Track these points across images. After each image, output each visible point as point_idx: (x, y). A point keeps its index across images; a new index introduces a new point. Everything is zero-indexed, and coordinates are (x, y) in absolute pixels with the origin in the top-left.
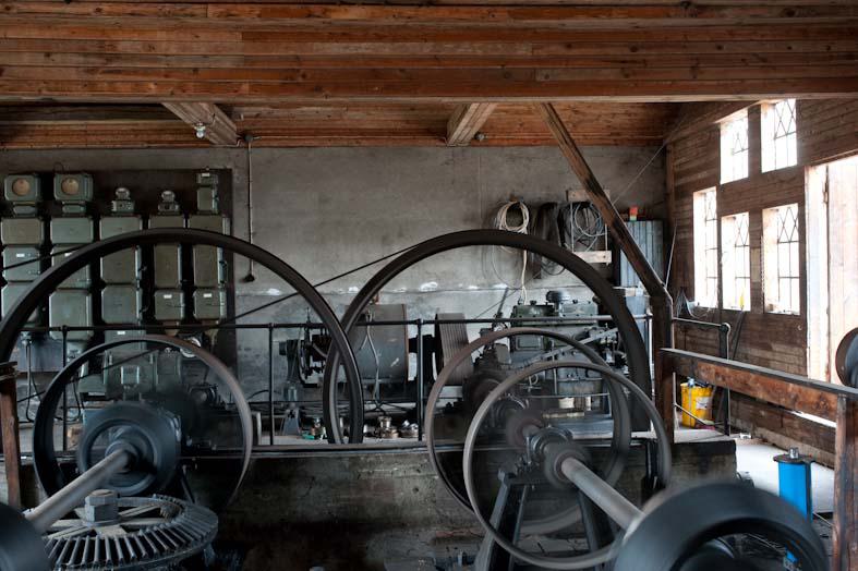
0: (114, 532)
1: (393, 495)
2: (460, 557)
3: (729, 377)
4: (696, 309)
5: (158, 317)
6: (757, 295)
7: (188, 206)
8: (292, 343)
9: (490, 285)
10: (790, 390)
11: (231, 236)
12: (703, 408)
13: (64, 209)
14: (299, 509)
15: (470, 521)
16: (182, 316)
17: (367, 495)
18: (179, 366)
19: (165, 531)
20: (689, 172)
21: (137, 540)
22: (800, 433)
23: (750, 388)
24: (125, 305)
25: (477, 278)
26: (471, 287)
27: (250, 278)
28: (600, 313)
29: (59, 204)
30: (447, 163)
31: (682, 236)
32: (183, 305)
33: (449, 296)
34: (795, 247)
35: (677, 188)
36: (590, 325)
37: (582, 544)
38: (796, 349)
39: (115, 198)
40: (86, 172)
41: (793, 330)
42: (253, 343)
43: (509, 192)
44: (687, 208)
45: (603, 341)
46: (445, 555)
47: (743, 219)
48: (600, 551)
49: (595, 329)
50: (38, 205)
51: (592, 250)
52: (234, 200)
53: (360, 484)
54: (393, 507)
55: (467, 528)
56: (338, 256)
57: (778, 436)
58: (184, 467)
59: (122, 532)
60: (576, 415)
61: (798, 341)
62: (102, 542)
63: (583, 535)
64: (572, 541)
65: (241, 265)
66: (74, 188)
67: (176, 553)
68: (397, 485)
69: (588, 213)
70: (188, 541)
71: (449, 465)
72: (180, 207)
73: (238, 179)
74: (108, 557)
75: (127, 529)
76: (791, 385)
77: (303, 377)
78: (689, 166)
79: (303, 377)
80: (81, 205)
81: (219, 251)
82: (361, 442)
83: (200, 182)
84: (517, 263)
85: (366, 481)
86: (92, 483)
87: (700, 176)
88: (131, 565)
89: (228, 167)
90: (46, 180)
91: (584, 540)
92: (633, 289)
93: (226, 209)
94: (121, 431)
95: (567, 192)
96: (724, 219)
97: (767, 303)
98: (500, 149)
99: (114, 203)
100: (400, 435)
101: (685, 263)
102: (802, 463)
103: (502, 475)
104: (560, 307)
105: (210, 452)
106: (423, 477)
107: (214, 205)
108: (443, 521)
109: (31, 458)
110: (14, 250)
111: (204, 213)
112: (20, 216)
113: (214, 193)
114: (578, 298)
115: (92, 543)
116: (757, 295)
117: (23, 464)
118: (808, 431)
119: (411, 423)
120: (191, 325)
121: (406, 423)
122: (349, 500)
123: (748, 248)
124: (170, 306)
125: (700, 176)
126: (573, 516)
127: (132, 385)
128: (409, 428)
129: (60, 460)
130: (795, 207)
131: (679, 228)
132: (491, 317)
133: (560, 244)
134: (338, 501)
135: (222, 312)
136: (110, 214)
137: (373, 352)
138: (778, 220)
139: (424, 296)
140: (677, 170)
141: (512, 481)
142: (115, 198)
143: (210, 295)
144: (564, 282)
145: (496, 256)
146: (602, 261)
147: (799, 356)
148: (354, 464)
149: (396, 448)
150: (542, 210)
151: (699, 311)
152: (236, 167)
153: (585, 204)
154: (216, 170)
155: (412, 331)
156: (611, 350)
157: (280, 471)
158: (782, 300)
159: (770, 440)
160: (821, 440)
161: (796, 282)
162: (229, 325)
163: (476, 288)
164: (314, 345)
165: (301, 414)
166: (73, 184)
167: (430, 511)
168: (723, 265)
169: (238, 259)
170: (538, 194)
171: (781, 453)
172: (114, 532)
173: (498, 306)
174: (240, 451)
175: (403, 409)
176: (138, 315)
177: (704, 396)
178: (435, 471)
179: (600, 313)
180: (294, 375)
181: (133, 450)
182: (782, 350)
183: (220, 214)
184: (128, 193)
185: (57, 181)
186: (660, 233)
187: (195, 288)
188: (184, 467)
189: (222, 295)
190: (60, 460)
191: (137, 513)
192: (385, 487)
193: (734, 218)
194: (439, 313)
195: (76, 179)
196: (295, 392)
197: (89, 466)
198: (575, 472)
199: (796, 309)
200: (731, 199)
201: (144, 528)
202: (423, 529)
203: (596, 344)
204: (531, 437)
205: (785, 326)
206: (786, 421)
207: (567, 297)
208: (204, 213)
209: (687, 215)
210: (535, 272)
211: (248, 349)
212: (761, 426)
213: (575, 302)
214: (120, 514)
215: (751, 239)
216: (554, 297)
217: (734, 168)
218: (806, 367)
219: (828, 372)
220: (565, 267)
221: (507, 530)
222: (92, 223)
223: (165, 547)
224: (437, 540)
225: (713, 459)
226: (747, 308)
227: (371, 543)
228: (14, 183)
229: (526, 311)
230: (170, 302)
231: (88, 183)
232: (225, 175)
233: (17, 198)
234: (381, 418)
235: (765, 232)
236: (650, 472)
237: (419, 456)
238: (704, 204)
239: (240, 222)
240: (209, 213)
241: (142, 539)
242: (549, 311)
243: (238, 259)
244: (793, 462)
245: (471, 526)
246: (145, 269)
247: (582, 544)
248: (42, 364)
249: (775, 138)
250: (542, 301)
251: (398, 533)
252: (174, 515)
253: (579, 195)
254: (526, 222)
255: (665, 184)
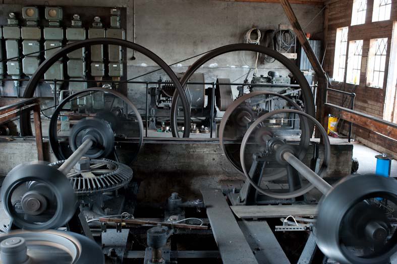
0: (88, 175)
1: (204, 161)
2: (234, 190)
3: (357, 119)
4: (333, 82)
5: (93, 74)
6: (363, 78)
7: (106, 25)
8: (153, 89)
9: (241, 66)
10: (387, 128)
11: (126, 40)
12: (333, 126)
13: (50, 23)
14: (163, 165)
15: (236, 173)
16: (103, 74)
17: (192, 161)
18: (103, 97)
19: (112, 176)
20: (336, 19)
21: (101, 179)
22: (377, 141)
23: (367, 125)
24: (77, 69)
25: (236, 62)
26: (232, 67)
27: (133, 58)
28: (291, 84)
29: (48, 21)
30: (225, 9)
31: (329, 48)
32: (104, 70)
33: (222, 70)
34: (384, 58)
35: (329, 26)
36: (287, 87)
37: (286, 186)
38: (379, 104)
39: (73, 19)
40: (60, 6)
41: (379, 95)
42: (137, 89)
43: (252, 24)
44: (333, 35)
45: (292, 95)
46: (226, 189)
47: (360, 43)
48: (295, 192)
49: (289, 89)
50: (38, 21)
51: (288, 52)
52: (127, 21)
53: (190, 156)
54: (203, 166)
55: (235, 176)
56: (173, 50)
57: (367, 141)
58: (115, 147)
59: (93, 176)
60: (277, 126)
61: (381, 100)
62: (86, 180)
63: (286, 182)
64: (281, 184)
65: (130, 53)
66: (54, 14)
67: (117, 186)
68: (205, 157)
69: (287, 35)
70: (122, 181)
71: (232, 151)
72: (103, 24)
73: (129, 12)
74: (89, 187)
75: (96, 175)
76: (389, 127)
77: (157, 103)
78: (337, 16)
79: (157, 103)
80: (57, 22)
81: (120, 47)
82: (188, 136)
83: (112, 13)
84: (254, 57)
85: (192, 155)
86: (80, 155)
87: (341, 21)
88: (99, 190)
89: (125, 6)
90: (41, 9)
91: (287, 185)
92: (307, 72)
93: (123, 26)
94: (88, 130)
95: (279, 25)
96: (350, 42)
97: (367, 82)
98: (248, 3)
99: (73, 21)
100: (200, 132)
101: (330, 60)
102: (388, 159)
103: (255, 157)
104: (274, 78)
105: (124, 139)
106: (217, 154)
107: (118, 24)
108: (224, 173)
109: (48, 139)
110: (28, 41)
111: (113, 28)
112: (30, 26)
113: (118, 19)
114: (283, 75)
115: (82, 180)
116: (363, 78)
117: (44, 141)
118: (381, 140)
119: (205, 126)
120: (107, 78)
121: (203, 127)
122: (184, 162)
123: (361, 57)
124: (98, 70)
125: (341, 21)
126: (282, 174)
127: (82, 105)
128: (204, 129)
129: (59, 140)
130: (386, 40)
131: (329, 44)
132: (243, 83)
133: (274, 49)
134: (180, 162)
135: (121, 74)
136: (70, 26)
137: (192, 94)
138: (378, 45)
139: (211, 70)
140: (329, 17)
141: (259, 160)
142: (73, 19)
143: (116, 66)
144: (274, 66)
145: (244, 55)
146: (292, 58)
147: (380, 107)
148: (187, 148)
149: (206, 141)
150: (267, 33)
151: (334, 83)
152: (128, 6)
153: (287, 31)
154: (119, 8)
155: (207, 87)
156: (295, 99)
157: (156, 148)
158: (375, 81)
159: (362, 142)
160: (387, 145)
161: (382, 74)
162: (124, 80)
163: (234, 67)
164: (163, 91)
165: (156, 120)
166: (54, 12)
167: (219, 169)
168: (348, 62)
169: (128, 49)
170: (265, 25)
171: (379, 154)
172: (88, 175)
173: (246, 76)
174: (139, 140)
175: (200, 119)
176: (84, 73)
177: (334, 121)
178: (223, 152)
179: (291, 84)
180: (153, 102)
181: (95, 139)
182: (373, 104)
183: (121, 28)
184: (79, 17)
185: (46, 10)
186: (319, 46)
187: (109, 62)
188: (115, 147)
189: (121, 66)
190: (59, 140)
191: (97, 167)
192: (201, 158)
193: (342, 29)
194: (219, 77)
195: (55, 10)
196: (154, 111)
197: (76, 148)
198: (287, 157)
199: (381, 86)
200: (355, 33)
201: (103, 174)
202: (216, 176)
203: (289, 96)
204: (269, 141)
205: (375, 93)
206: (371, 135)
207: (277, 74)
208: (113, 28)
209: (333, 38)
210: (262, 61)
211: (132, 90)
212: (359, 136)
213: (280, 77)
214: (91, 167)
215: (363, 53)
216: (272, 74)
217: (358, 18)
218: (383, 112)
219: (392, 115)
220: (276, 59)
221: (256, 179)
222: (62, 30)
223: (113, 183)
224: (221, 181)
225: (343, 152)
226: (358, 83)
227: (193, 181)
228: (27, 10)
229: (258, 80)
230: (98, 68)
231: (61, 11)
232: (123, 10)
233: (29, 18)
234: (192, 124)
235: (370, 50)
236: (315, 156)
237: (216, 145)
238: (342, 34)
239: (129, 32)
240: (116, 28)
241: (102, 179)
242: (269, 80)
243: (128, 49)
244: (385, 159)
245: (237, 176)
246: (87, 52)
247: (286, 186)
248: (41, 95)
249: (380, 6)
250: (266, 75)
251: (205, 177)
252: (114, 168)
253: (286, 25)
254: (259, 38)
255: (323, 23)
